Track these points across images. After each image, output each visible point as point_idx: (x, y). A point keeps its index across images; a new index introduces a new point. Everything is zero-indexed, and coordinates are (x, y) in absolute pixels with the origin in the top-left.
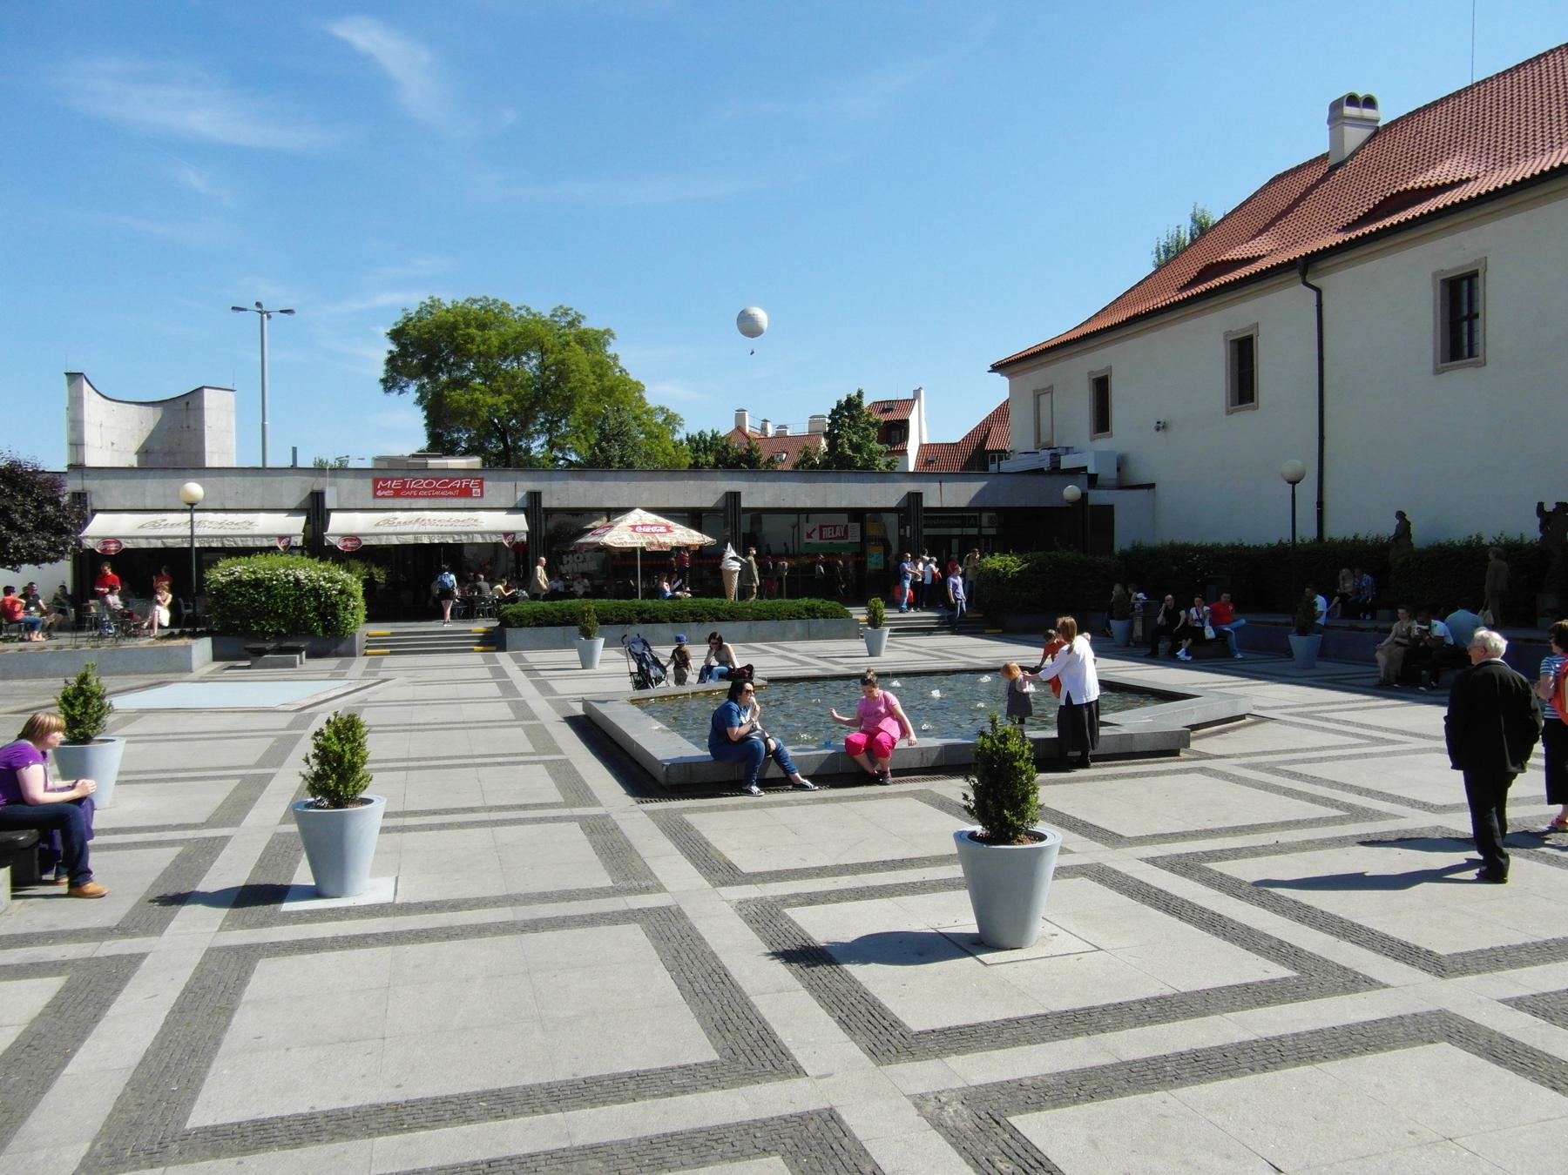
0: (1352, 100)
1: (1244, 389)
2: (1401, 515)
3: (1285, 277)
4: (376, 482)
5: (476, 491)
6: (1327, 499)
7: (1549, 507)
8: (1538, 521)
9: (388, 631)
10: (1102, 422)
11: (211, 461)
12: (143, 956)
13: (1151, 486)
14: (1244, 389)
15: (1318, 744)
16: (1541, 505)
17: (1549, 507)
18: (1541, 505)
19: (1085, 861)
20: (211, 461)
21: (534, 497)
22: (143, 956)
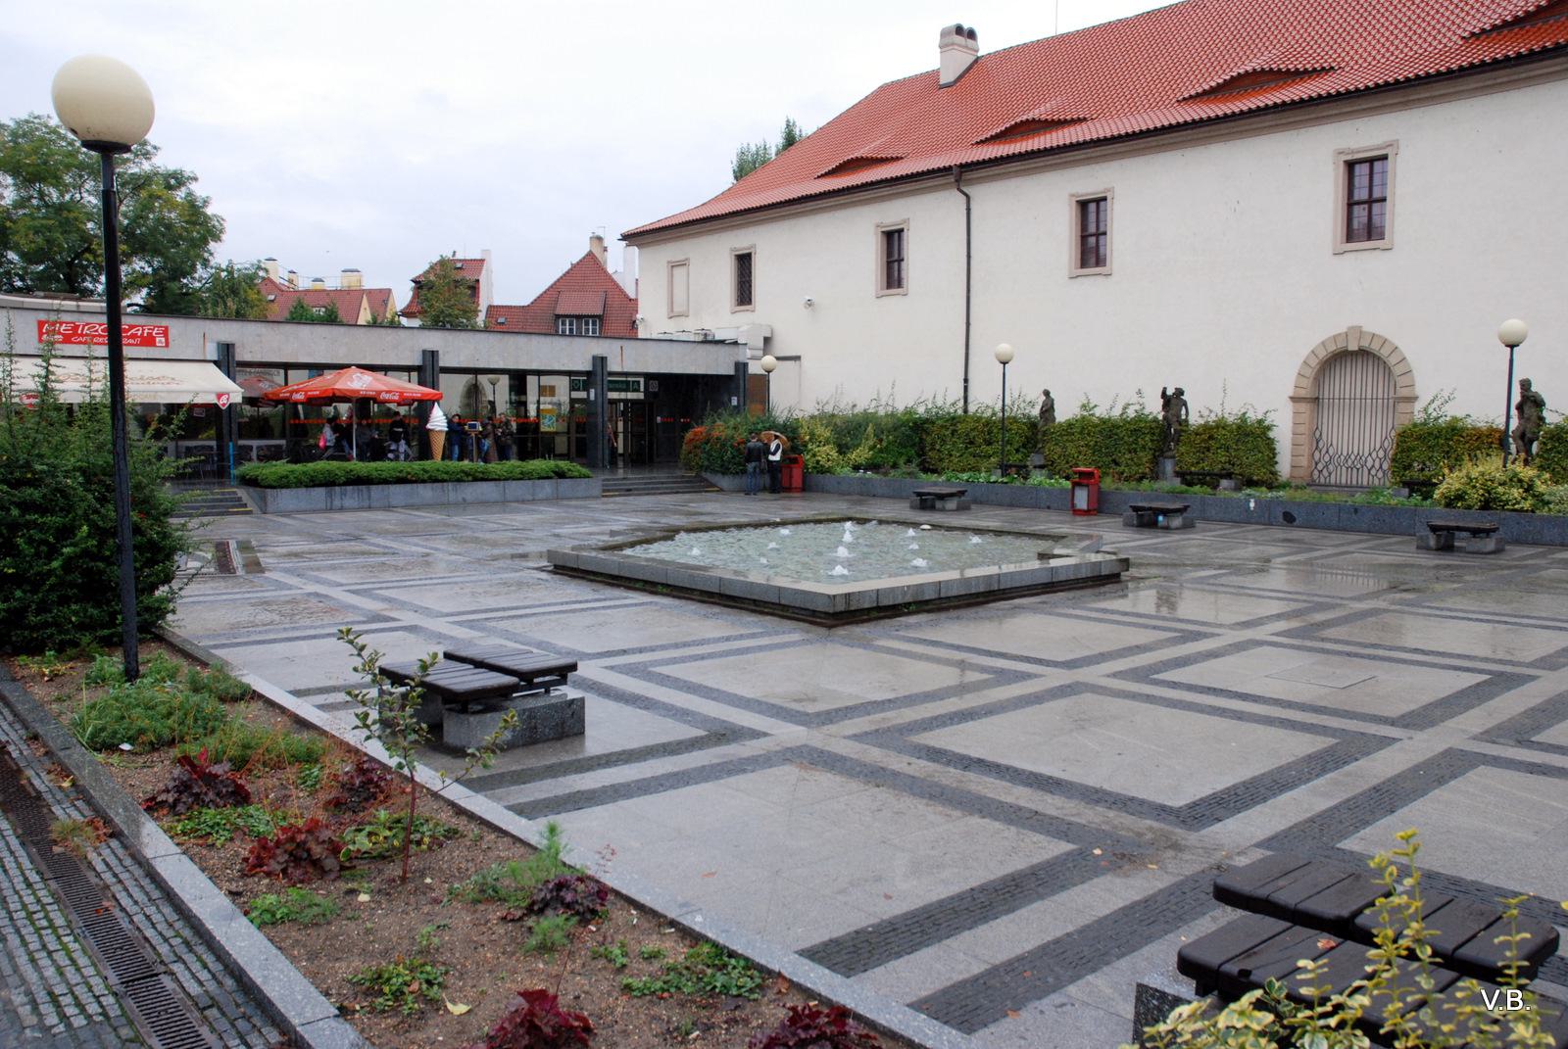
0: (959, 30)
1: (893, 275)
2: (1047, 393)
3: (941, 181)
4: (41, 324)
5: (160, 340)
6: (971, 376)
7: (1170, 392)
8: (1161, 402)
9: (1233, 553)
10: (744, 294)
11: (641, 335)
12: (918, 1006)
13: (797, 358)
14: (893, 275)
15: (390, 590)
16: (1165, 390)
17: (1170, 392)
18: (1165, 390)
19: (833, 728)
20: (641, 335)
21: (227, 349)
22: (918, 1006)
